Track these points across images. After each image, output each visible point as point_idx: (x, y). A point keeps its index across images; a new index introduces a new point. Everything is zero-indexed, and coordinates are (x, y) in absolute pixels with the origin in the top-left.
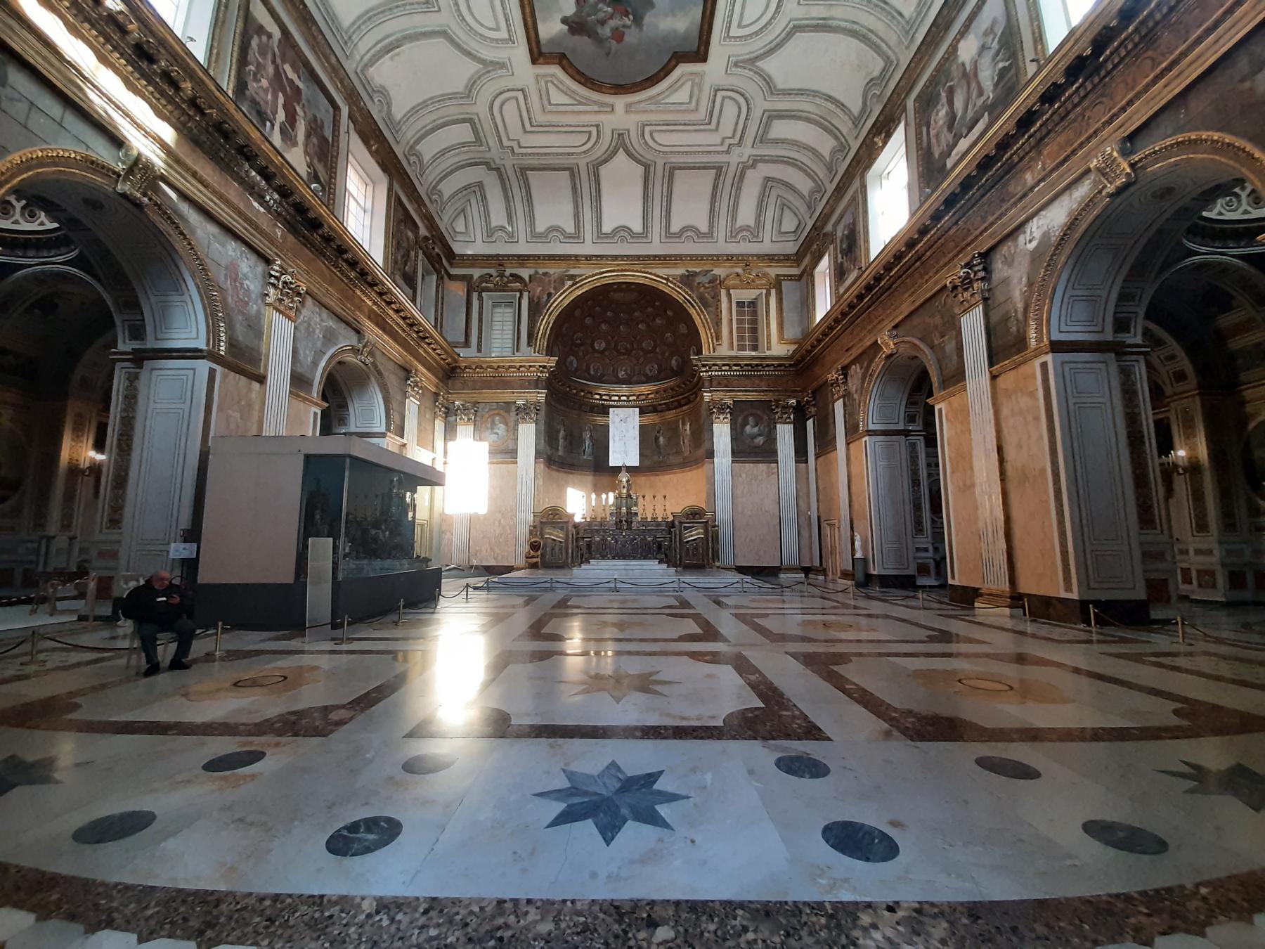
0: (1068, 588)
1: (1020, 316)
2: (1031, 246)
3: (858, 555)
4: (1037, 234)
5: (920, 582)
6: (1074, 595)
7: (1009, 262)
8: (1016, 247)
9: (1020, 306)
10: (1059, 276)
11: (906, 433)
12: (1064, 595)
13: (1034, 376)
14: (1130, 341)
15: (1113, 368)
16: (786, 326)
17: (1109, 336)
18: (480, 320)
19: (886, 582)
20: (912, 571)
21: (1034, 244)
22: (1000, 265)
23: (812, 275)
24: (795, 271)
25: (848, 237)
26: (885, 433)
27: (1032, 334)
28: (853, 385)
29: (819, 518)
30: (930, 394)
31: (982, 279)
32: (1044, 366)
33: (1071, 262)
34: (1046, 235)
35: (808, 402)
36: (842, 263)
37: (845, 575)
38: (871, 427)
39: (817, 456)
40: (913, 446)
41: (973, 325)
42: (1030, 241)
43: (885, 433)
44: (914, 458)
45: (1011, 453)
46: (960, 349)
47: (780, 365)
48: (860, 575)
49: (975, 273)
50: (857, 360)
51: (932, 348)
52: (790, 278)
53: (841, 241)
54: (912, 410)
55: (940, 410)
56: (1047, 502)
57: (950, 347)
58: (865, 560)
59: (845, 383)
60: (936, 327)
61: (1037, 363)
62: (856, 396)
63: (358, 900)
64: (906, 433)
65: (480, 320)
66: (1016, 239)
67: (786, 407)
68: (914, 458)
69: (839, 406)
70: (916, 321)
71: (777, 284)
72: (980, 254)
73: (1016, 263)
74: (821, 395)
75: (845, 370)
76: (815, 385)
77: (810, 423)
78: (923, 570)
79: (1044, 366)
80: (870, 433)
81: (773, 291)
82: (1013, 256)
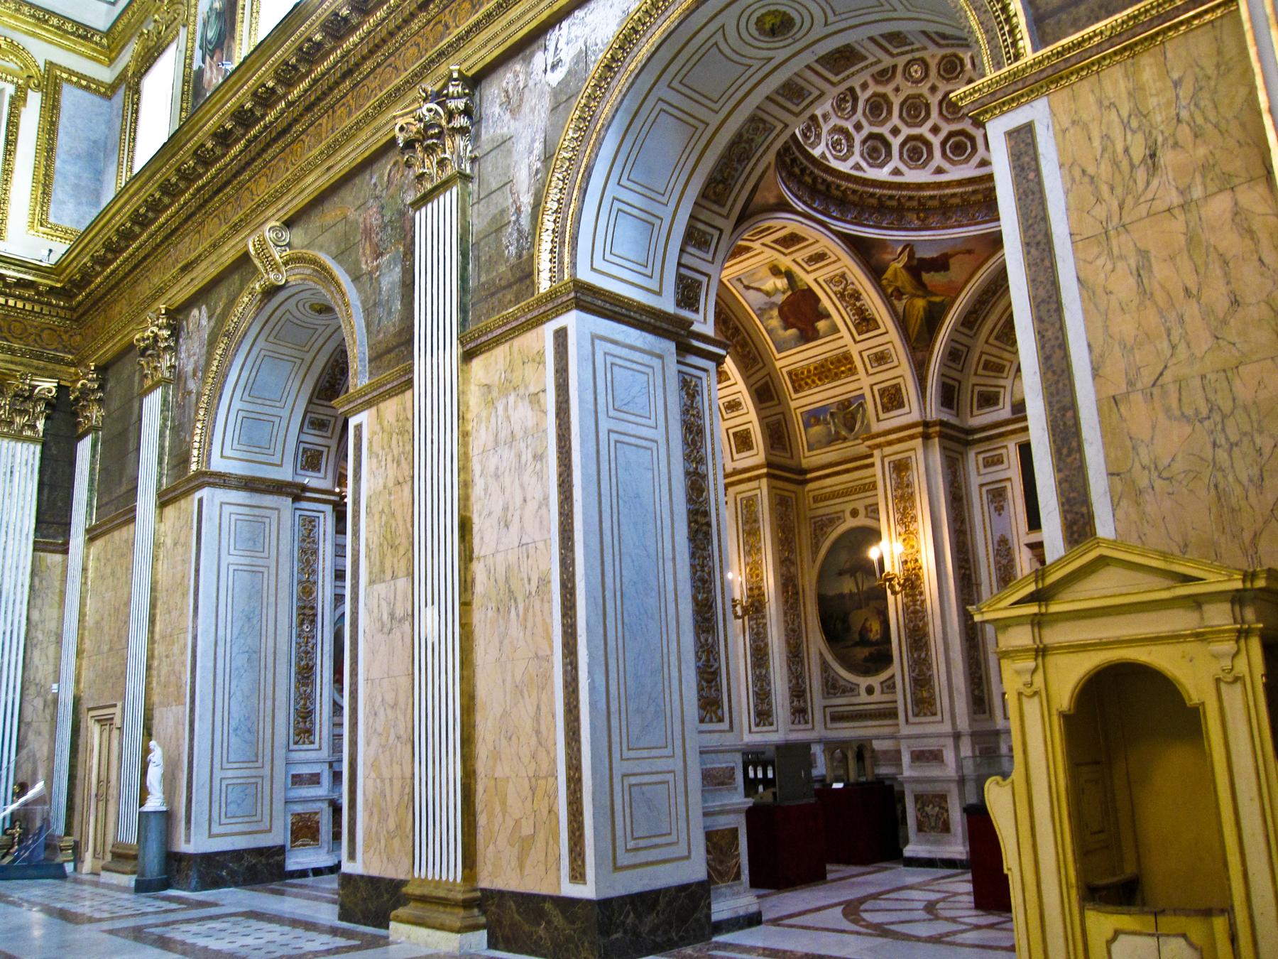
0: (578, 875)
1: (525, 222)
2: (555, 77)
3: (155, 803)
4: (568, 55)
5: (295, 861)
6: (586, 891)
7: (513, 105)
8: (529, 74)
9: (526, 200)
10: (599, 142)
11: (297, 493)
12: (570, 890)
13: (539, 359)
14: (696, 327)
15: (673, 367)
16: (58, 192)
17: (667, 304)
18: (726, 646)
19: (217, 870)
20: (278, 836)
21: (560, 74)
22: (497, 110)
23: (137, 91)
24: (105, 75)
25: (219, 15)
26: (249, 485)
27: (544, 263)
28: (190, 353)
29: (77, 701)
30: (751, 814)
31: (463, 131)
32: (561, 335)
33: (631, 104)
34: (583, 56)
35: (85, 392)
36: (200, 72)
37: (122, 858)
38: (217, 465)
39: (93, 535)
40: (310, 524)
41: (436, 226)
42: (554, 67)
43: (249, 485)
44: (308, 554)
45: (485, 536)
46: (408, 285)
47: (21, 283)
48: (152, 862)
49: (451, 115)
50: (201, 296)
51: (356, 279)
52: (88, 84)
53: (205, 25)
54: (313, 438)
55: (358, 428)
56: (548, 659)
57: (390, 279)
58: (167, 817)
59: (174, 350)
60: (367, 232)
61: (549, 328)
62: (192, 385)
63: (822, 325)
64: (297, 493)
65: (726, 646)
66: (528, 61)
67: (28, 396)
68: (308, 554)
69: (152, 405)
70: (330, 213)
71: (51, 83)
72: (462, 77)
73: (526, 108)
74: (120, 372)
75: (176, 317)
76: (109, 349)
77: (84, 449)
78: (305, 830)
79: (561, 335)
80: (222, 481)
81: (34, 100)
82: (521, 93)
